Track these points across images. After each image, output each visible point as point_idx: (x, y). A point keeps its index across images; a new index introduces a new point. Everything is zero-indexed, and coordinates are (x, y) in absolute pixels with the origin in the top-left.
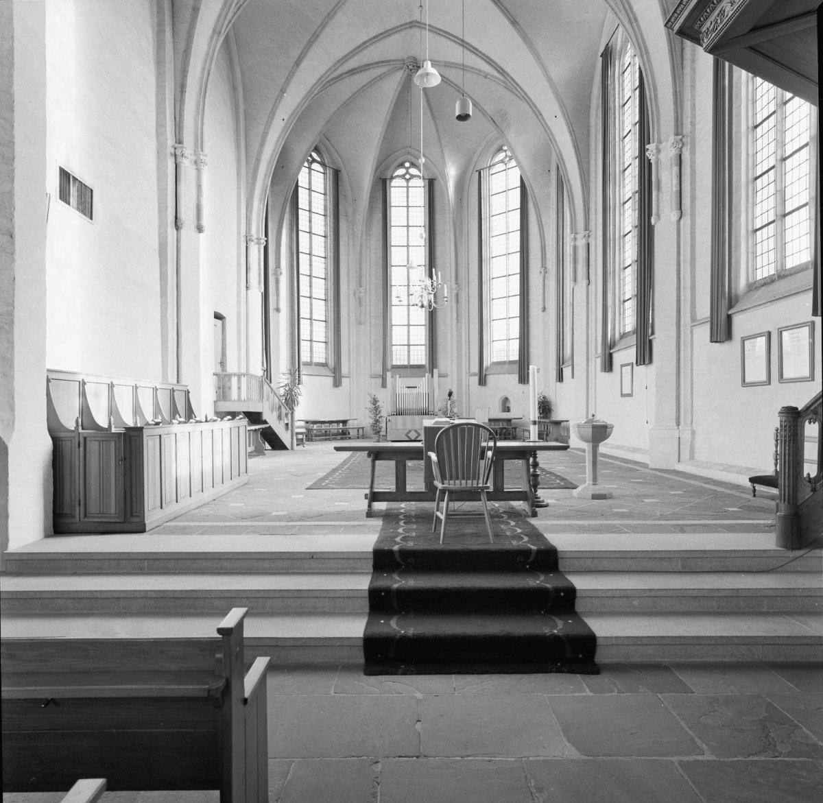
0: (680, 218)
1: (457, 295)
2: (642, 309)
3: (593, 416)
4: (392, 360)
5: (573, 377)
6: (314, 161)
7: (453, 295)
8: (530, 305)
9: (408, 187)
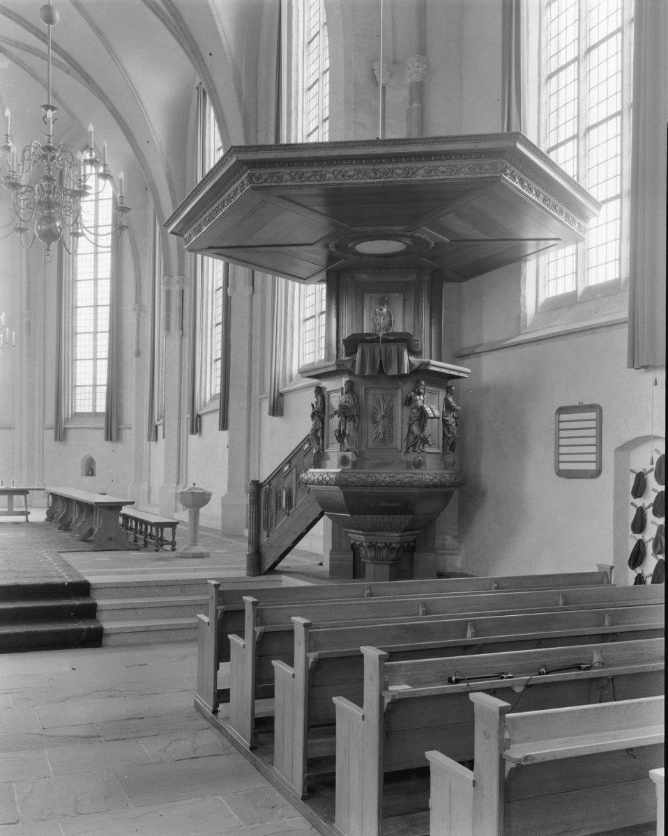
0: (253, 293)
1: (29, 324)
2: (203, 384)
3: (194, 484)
5: (164, 438)
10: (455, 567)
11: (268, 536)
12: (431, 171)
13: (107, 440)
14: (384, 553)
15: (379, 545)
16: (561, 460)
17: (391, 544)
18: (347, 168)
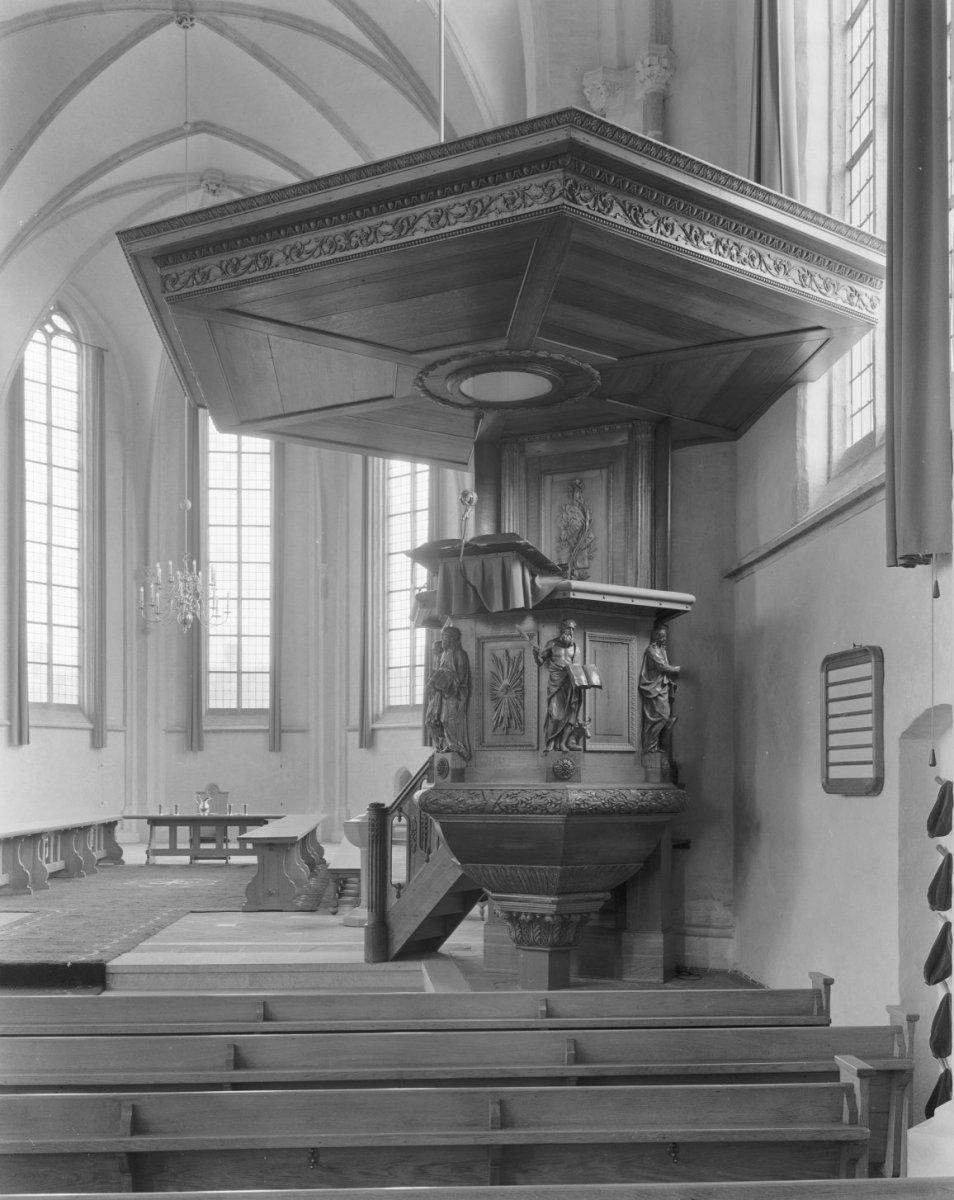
1: (326, 582)
4: (207, 701)
6: (58, 331)
7: (320, 581)
8: (151, 1082)
9: (239, 453)
10: (725, 960)
11: (398, 896)
12: (438, 218)
13: (426, 745)
14: (535, 933)
15: (523, 917)
16: (832, 759)
17: (543, 916)
18: (304, 239)
